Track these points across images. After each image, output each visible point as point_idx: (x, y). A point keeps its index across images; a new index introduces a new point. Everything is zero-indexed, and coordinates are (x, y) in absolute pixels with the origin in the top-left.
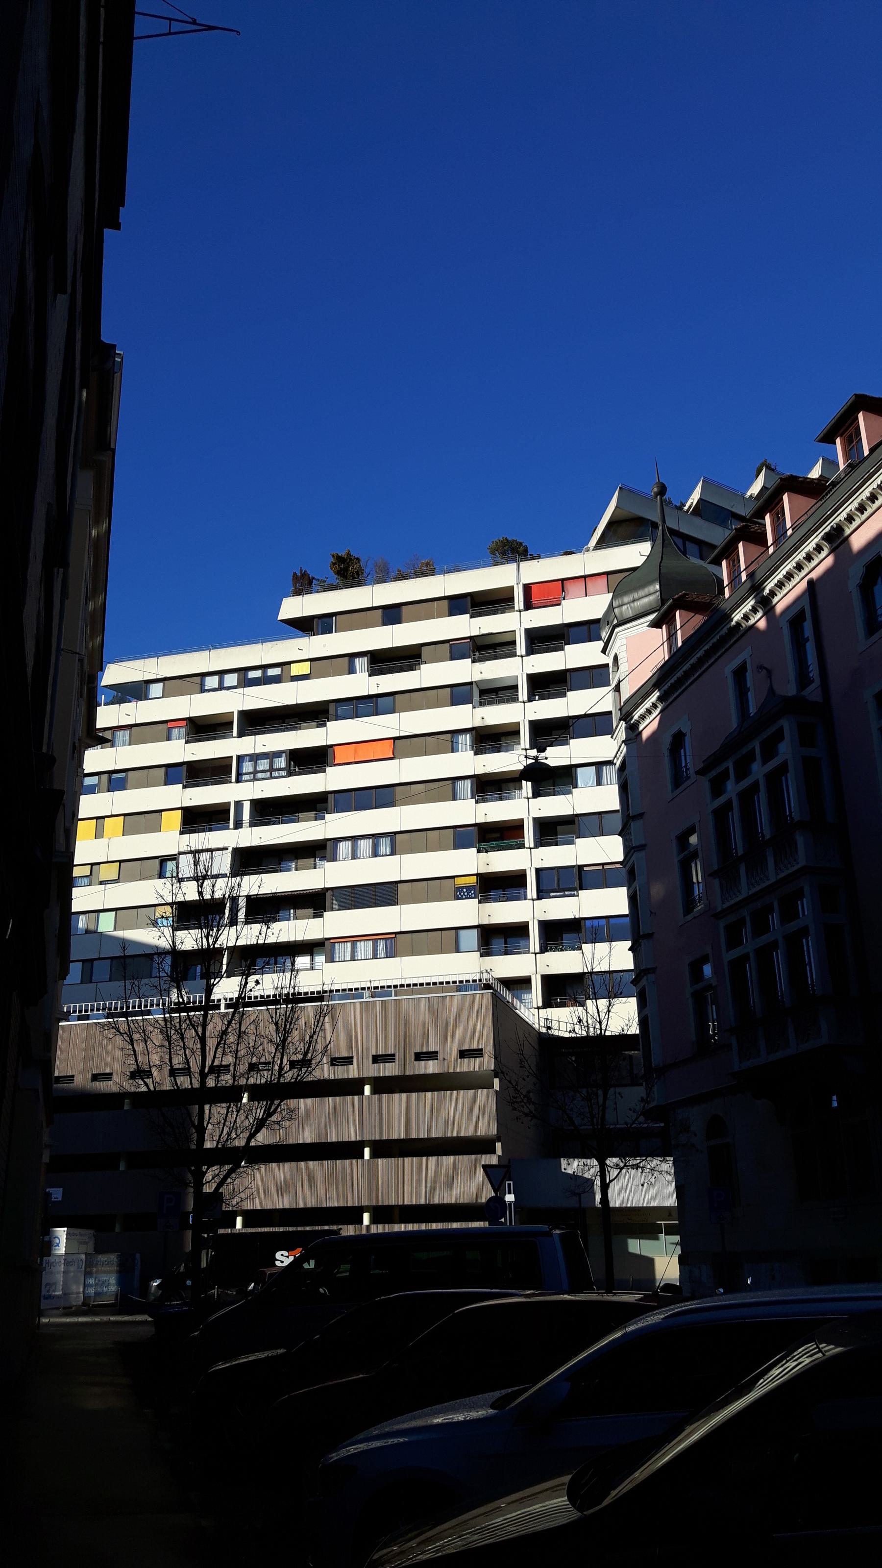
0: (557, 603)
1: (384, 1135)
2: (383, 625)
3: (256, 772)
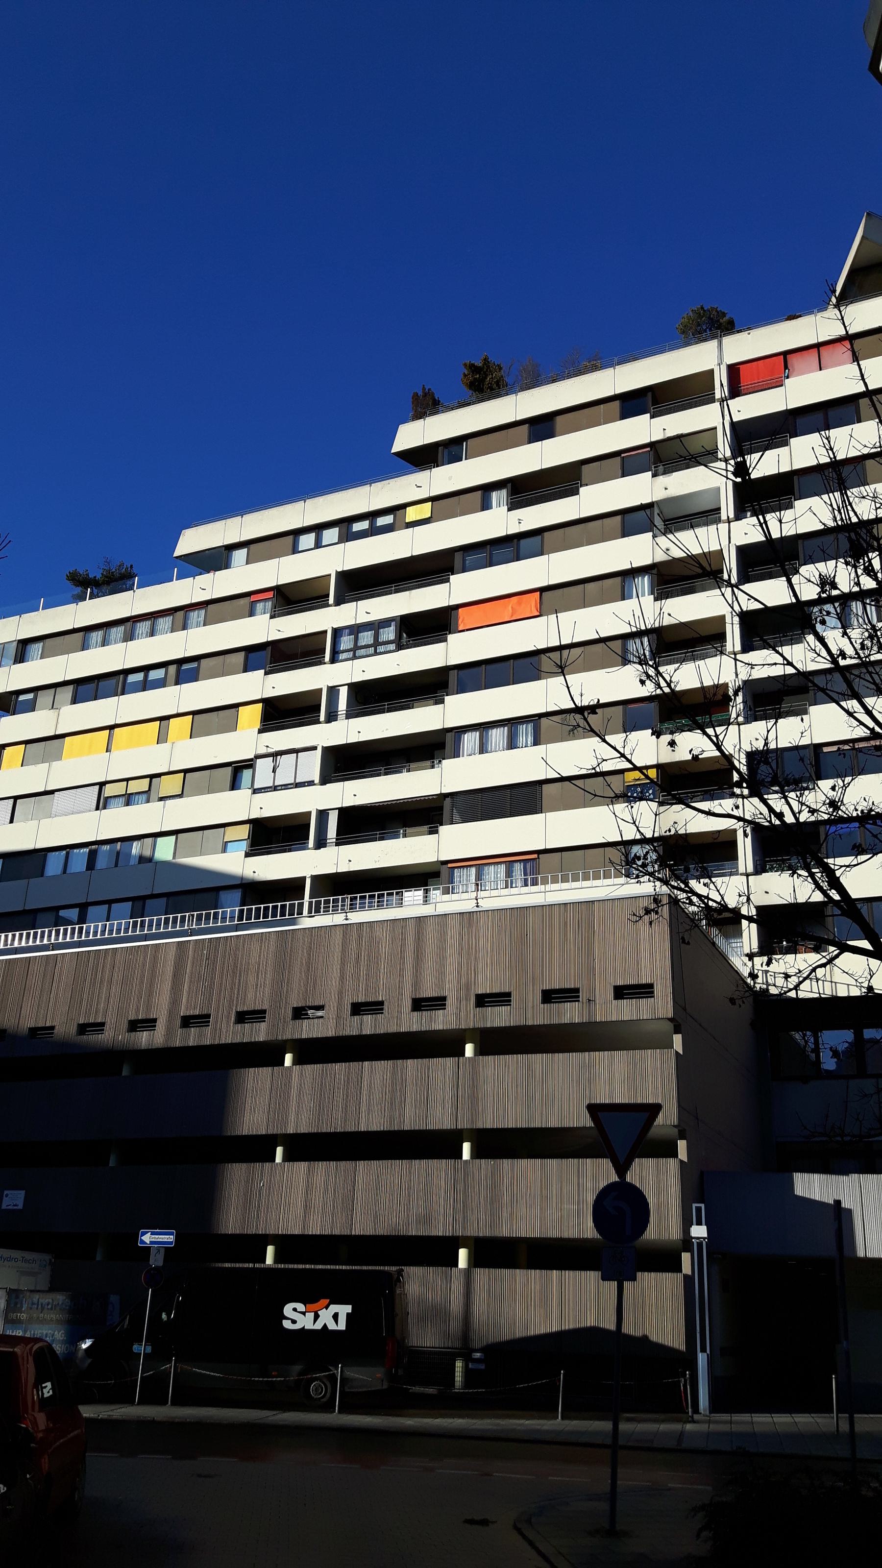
0: (779, 384)
1: (489, 1121)
2: (530, 443)
3: (356, 648)
